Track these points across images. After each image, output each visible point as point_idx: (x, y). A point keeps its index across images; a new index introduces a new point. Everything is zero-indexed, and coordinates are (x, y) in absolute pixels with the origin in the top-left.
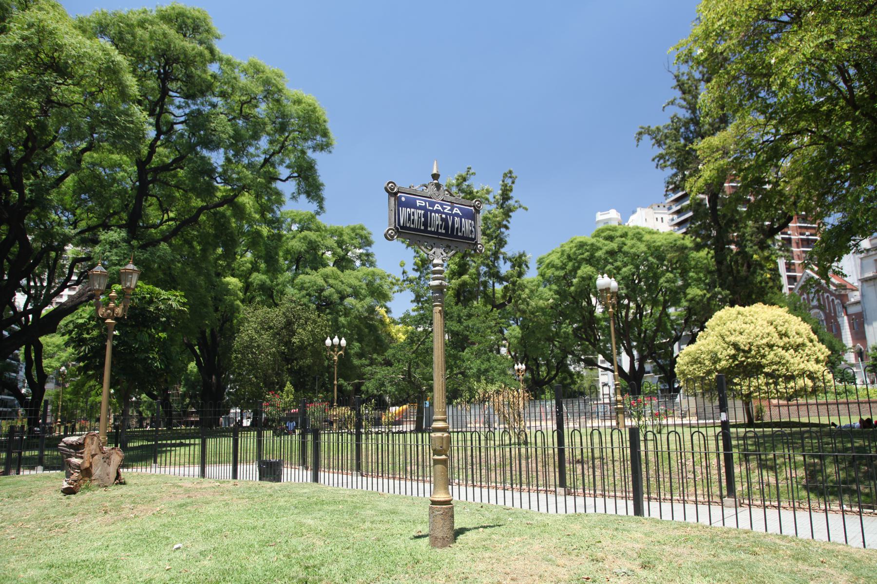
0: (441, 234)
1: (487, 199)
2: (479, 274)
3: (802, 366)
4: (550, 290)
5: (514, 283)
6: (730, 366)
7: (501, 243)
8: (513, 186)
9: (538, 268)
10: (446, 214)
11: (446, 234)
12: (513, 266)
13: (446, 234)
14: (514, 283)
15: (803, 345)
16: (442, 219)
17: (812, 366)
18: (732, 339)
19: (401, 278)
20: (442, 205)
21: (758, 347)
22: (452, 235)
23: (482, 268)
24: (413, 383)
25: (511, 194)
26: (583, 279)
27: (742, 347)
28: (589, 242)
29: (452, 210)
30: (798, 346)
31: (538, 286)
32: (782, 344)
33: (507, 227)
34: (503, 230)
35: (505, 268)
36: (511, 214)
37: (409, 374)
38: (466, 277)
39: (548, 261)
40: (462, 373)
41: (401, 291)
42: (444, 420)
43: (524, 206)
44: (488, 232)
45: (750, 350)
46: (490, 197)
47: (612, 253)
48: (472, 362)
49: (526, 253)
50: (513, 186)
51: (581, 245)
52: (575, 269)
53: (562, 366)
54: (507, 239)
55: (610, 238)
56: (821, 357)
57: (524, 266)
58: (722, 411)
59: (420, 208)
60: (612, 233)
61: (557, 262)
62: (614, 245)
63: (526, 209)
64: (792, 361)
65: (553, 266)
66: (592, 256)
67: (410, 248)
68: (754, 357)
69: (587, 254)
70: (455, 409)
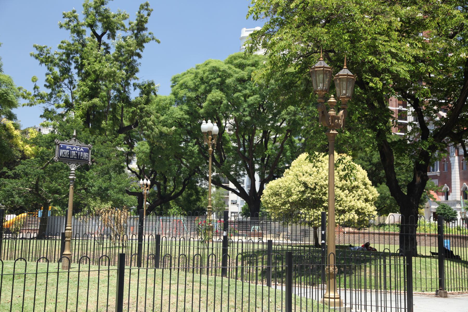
0: (75, 159)
1: (123, 26)
2: (109, 98)
3: (353, 203)
4: (181, 109)
5: (141, 109)
6: (300, 200)
7: (132, 70)
8: (149, 18)
9: (172, 87)
10: (78, 151)
11: (77, 159)
12: (142, 92)
13: (77, 159)
14: (141, 109)
15: (358, 187)
16: (76, 153)
17: (360, 204)
18: (303, 179)
19: (32, 93)
20: (76, 147)
21: (322, 187)
22: (79, 159)
23: (112, 91)
24: (40, 196)
25: (146, 26)
26: (213, 103)
27: (310, 186)
28: (222, 69)
29: (80, 149)
30: (353, 188)
31: (171, 104)
32: (340, 185)
33: (139, 56)
34: (136, 58)
35: (134, 95)
36: (144, 44)
37: (36, 188)
38: (96, 100)
39: (181, 82)
40: (86, 189)
41: (31, 105)
42: (71, 226)
43: (157, 38)
44: (121, 58)
45: (315, 188)
46: (125, 23)
47: (241, 81)
48: (95, 181)
49: (155, 83)
50: (149, 18)
51: (214, 70)
52: (207, 92)
53: (189, 183)
54: (139, 67)
55: (242, 66)
56: (371, 197)
57: (152, 94)
58: (224, 230)
59: (68, 149)
60: (244, 61)
61: (191, 84)
62: (244, 74)
63: (159, 42)
64: (345, 199)
65: (187, 87)
66: (223, 82)
67: (43, 65)
68: (317, 194)
69: (218, 79)
70: (76, 221)
